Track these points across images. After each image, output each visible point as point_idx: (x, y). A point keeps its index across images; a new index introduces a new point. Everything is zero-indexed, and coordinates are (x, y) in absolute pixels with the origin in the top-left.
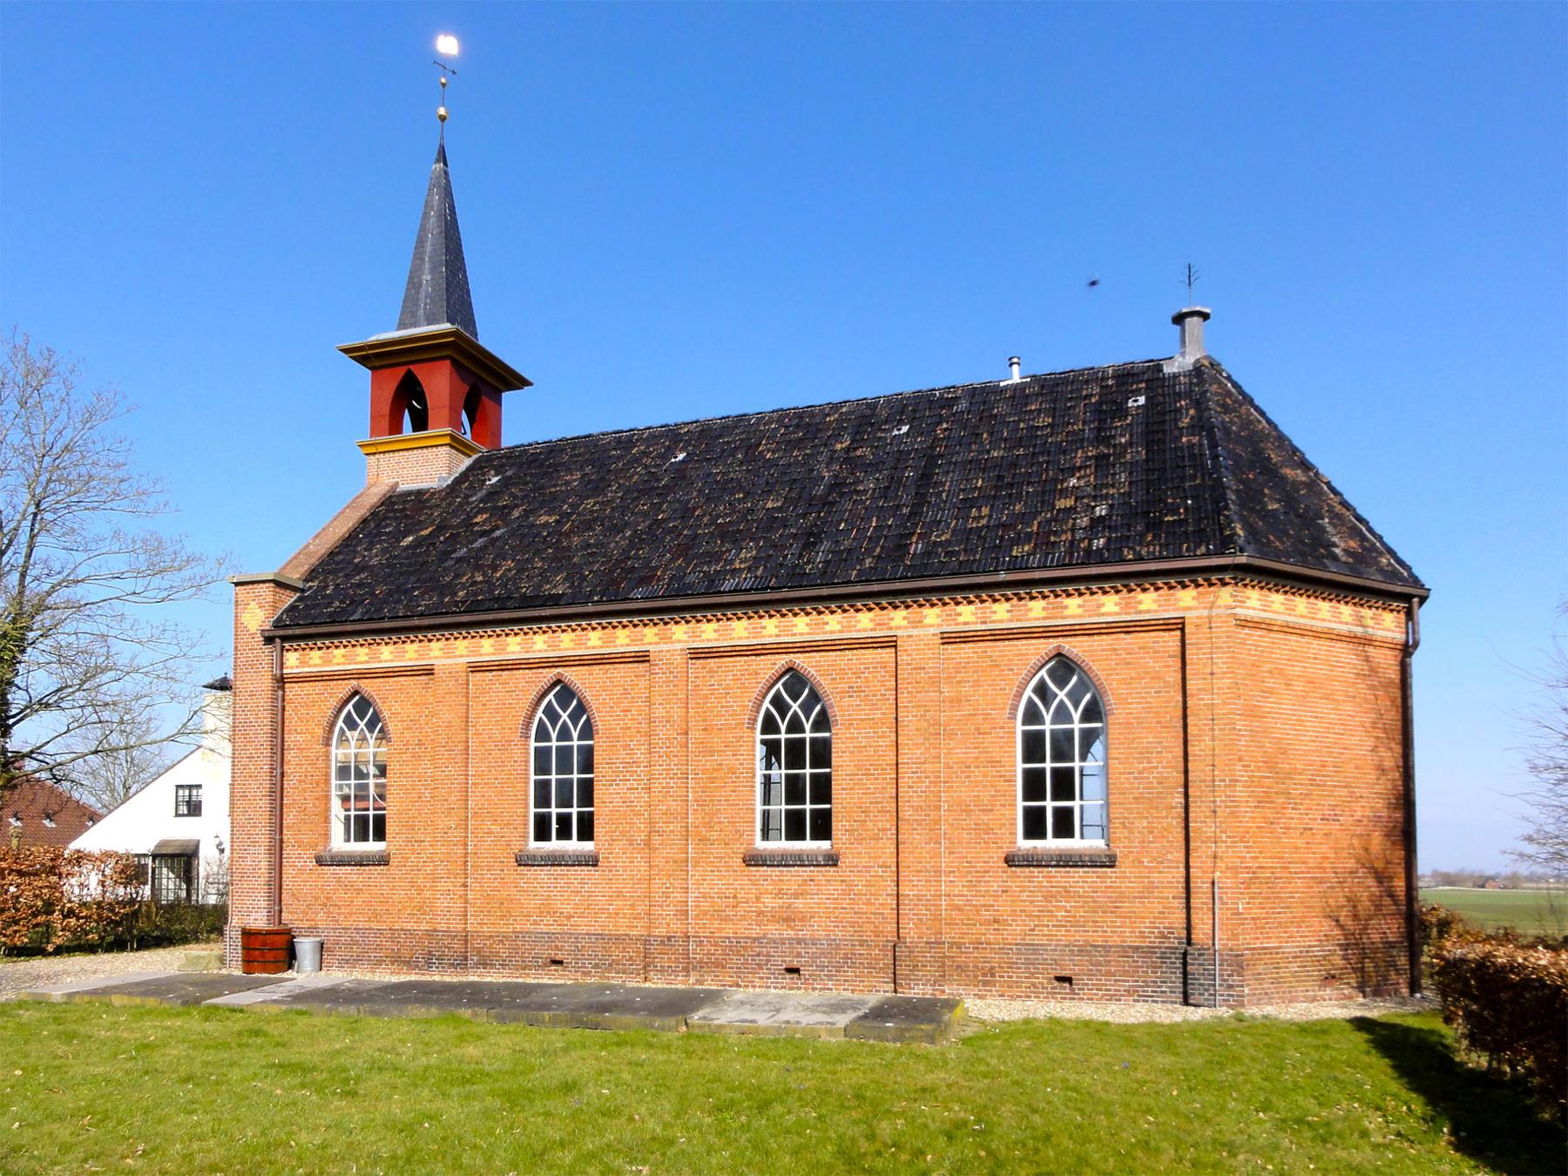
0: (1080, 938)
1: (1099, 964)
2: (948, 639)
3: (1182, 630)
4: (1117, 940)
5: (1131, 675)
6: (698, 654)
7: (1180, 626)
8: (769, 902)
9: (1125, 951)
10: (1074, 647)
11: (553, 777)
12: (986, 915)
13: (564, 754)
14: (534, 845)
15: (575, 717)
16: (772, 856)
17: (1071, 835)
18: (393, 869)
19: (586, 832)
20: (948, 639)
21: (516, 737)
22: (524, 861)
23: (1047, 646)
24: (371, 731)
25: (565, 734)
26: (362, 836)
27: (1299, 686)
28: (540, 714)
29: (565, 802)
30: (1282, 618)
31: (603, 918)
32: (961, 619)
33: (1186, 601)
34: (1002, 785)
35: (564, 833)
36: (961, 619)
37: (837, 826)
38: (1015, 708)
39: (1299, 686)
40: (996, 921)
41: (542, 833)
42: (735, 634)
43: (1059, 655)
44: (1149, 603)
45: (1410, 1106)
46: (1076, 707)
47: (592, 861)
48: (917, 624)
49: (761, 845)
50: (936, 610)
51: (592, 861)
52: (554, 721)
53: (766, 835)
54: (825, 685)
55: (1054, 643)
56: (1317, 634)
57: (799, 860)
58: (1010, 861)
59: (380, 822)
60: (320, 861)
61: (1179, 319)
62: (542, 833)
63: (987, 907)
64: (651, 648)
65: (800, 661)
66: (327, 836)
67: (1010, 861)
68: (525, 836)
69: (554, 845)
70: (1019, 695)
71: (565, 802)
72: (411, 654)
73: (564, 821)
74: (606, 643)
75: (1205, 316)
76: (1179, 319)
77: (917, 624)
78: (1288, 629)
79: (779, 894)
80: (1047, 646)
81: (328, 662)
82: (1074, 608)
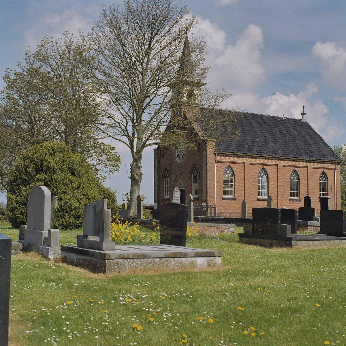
7: (307, 168)
20: (314, 168)
29: (323, 191)
33: (245, 160)
65: (296, 169)
72: (241, 160)
77: (310, 165)
80: (322, 171)
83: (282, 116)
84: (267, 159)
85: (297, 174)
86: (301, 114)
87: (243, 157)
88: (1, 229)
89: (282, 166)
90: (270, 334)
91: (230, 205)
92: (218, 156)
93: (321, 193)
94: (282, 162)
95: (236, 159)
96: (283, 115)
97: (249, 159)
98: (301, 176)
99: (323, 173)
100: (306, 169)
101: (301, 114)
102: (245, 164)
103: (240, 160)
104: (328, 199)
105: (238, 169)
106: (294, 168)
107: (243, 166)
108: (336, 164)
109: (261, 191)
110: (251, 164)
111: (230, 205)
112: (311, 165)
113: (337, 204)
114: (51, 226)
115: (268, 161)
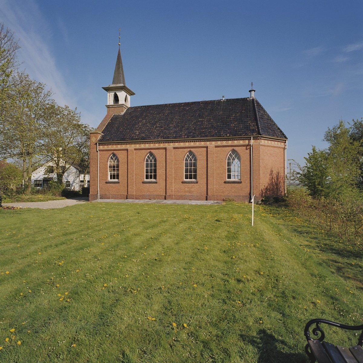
0: (236, 194)
1: (239, 198)
2: (216, 147)
3: (127, 151)
4: (242, 195)
5: (200, 154)
6: (174, 148)
9: (243, 197)
10: (236, 148)
11: (189, 168)
12: (222, 191)
13: (191, 164)
14: (146, 180)
15: (192, 157)
16: (187, 182)
17: (230, 178)
18: (120, 184)
19: (155, 178)
20: (216, 147)
21: (143, 161)
22: (143, 183)
24: (116, 160)
25: (191, 160)
26: (114, 178)
28: (147, 157)
29: (151, 172)
30: (267, 144)
31: (158, 192)
32: (218, 144)
33: (128, 147)
35: (151, 178)
36: (218, 144)
37: (198, 177)
38: (144, 159)
39: (269, 155)
40: (223, 192)
42: (181, 145)
43: (233, 149)
44: (162, 145)
46: (236, 158)
47: (156, 183)
49: (146, 180)
50: (143, 145)
51: (156, 183)
53: (111, 179)
54: (196, 154)
55: (233, 148)
56: (272, 147)
57: (192, 182)
58: (225, 182)
59: (118, 175)
60: (106, 183)
61: (250, 91)
62: (147, 178)
63: (222, 190)
64: (167, 147)
66: (107, 178)
67: (225, 182)
68: (144, 178)
70: (227, 156)
71: (151, 172)
72: (161, 145)
73: (151, 176)
74: (116, 147)
75: (255, 91)
76: (250, 91)
78: (268, 146)
80: (111, 152)
81: (116, 147)
82: (236, 143)
83: (222, 98)
84: (242, 140)
85: (194, 156)
87: (126, 143)
88: (357, 255)
91: (114, 188)
92: (253, 139)
94: (172, 144)
95: (119, 147)
97: (133, 145)
98: (199, 157)
103: (124, 147)
104: (152, 179)
105: (121, 156)
106: (189, 149)
107: (248, 151)
108: (251, 139)
110: (135, 149)
111: (114, 188)
112: (211, 145)
113: (255, 186)
115: (268, 143)
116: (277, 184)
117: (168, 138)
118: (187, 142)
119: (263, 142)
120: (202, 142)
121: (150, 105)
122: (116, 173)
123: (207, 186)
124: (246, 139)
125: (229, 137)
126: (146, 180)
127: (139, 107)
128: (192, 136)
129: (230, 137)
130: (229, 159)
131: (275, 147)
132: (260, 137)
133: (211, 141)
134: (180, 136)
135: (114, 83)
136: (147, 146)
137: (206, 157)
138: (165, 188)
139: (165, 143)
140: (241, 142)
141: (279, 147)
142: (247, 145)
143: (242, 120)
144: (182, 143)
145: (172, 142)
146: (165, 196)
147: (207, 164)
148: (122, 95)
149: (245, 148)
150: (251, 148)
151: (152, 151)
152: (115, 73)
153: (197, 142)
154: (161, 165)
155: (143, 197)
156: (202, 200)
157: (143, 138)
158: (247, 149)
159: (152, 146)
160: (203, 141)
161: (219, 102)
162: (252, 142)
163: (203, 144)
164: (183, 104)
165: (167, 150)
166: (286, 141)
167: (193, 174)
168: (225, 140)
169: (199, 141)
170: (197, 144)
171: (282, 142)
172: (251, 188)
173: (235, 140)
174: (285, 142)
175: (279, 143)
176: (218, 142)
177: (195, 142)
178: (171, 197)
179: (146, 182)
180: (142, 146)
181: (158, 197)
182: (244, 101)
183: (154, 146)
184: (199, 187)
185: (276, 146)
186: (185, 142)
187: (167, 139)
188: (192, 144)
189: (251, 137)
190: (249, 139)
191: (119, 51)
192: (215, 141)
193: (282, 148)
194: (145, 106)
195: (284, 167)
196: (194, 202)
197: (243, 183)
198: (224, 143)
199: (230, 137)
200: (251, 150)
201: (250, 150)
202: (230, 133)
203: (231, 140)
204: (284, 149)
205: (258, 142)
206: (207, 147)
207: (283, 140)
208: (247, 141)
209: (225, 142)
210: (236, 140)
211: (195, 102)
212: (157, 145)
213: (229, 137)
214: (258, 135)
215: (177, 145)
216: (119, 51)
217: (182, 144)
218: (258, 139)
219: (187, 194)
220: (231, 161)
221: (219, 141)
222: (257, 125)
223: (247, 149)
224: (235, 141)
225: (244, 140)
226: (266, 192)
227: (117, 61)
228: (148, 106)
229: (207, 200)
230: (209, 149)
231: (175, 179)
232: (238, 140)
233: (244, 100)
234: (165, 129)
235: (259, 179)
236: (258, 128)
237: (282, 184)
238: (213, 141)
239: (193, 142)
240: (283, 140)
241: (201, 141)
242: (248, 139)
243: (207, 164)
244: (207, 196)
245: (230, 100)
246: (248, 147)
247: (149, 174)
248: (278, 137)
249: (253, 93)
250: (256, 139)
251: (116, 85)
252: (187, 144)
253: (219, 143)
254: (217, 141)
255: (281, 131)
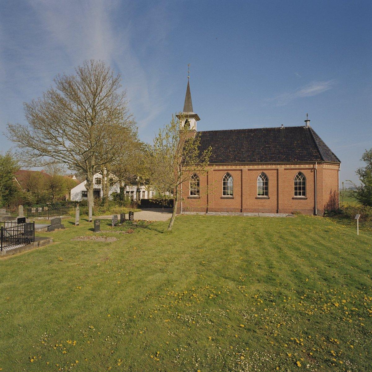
2: (285, 169)
5: (309, 175)
6: (249, 170)
7: (241, 170)
8: (259, 204)
12: (290, 205)
14: (223, 196)
20: (214, 170)
22: (221, 198)
23: (298, 171)
27: (328, 176)
33: (242, 167)
34: (292, 189)
37: (269, 194)
38: (222, 178)
41: (296, 194)
42: (255, 167)
44: (238, 167)
45: (70, 224)
48: (281, 167)
49: (223, 196)
52: (226, 178)
54: (267, 175)
56: (330, 169)
57: (264, 198)
58: (256, 198)
59: (198, 192)
60: (188, 198)
63: (290, 204)
65: (264, 171)
69: (298, 196)
75: (309, 121)
77: (281, 167)
79: (261, 203)
80: (298, 171)
83: (281, 126)
84: (308, 164)
86: (305, 121)
89: (247, 171)
90: (360, 316)
93: (265, 191)
94: (247, 167)
96: (282, 125)
98: (269, 178)
99: (300, 174)
100: (240, 171)
101: (305, 121)
102: (243, 170)
107: (313, 173)
108: (315, 164)
109: (226, 191)
112: (281, 168)
113: (318, 202)
114: (133, 215)
115: (332, 166)
116: (334, 201)
117: (244, 161)
118: (260, 165)
119: (325, 166)
120: (273, 166)
121: (217, 130)
122: (196, 190)
123: (278, 201)
124: (311, 164)
125: (297, 162)
126: (224, 196)
127: (207, 132)
128: (264, 160)
129: (298, 162)
130: (224, 180)
131: (332, 169)
132: (323, 162)
133: (281, 165)
134: (254, 160)
135: (184, 110)
136: (225, 168)
137: (276, 178)
138: (240, 203)
139: (241, 165)
140: (307, 166)
141: (335, 170)
142: (312, 169)
143: (299, 146)
144: (251, 166)
145: (248, 165)
146: (241, 210)
147: (278, 183)
148: (192, 121)
149: (310, 170)
150: (315, 171)
151: (229, 172)
152: (185, 102)
153: (269, 165)
154: (238, 183)
155: (221, 210)
156: (274, 213)
157: (221, 161)
158: (311, 172)
159: (229, 167)
160: (274, 165)
161: (279, 130)
162: (316, 166)
163: (274, 167)
164: (247, 131)
165: (243, 172)
166: (339, 164)
167: (302, 186)
168: (293, 164)
169: (271, 165)
170: (269, 167)
171: (337, 165)
172: (315, 203)
173: (301, 164)
174: (340, 165)
175: (335, 166)
176: (287, 165)
177: (267, 165)
178: (247, 211)
179: (223, 198)
180: (221, 168)
181: (234, 210)
182: (301, 129)
183: (231, 168)
184: (271, 202)
185: (333, 168)
186: (259, 165)
187: (242, 161)
188: (265, 167)
189: (316, 162)
190: (314, 164)
191: (188, 83)
192: (285, 165)
193: (336, 170)
194: (213, 131)
195: (338, 185)
196: (267, 215)
197: (308, 199)
198: (293, 167)
199: (298, 162)
200: (315, 173)
201: (315, 173)
202: (297, 158)
203: (298, 164)
204: (338, 170)
205: (321, 166)
206: (277, 170)
207: (338, 164)
208: (312, 166)
209: (293, 165)
210: (303, 164)
211: (257, 129)
212: (234, 167)
213: (297, 162)
214: (321, 160)
215: (251, 167)
216: (188, 83)
217: (256, 167)
218: (321, 164)
219: (260, 208)
220: (226, 181)
221: (288, 165)
222: (319, 151)
223: (311, 172)
224: (302, 165)
225: (309, 164)
226: (327, 208)
227: (187, 92)
228: (215, 131)
229: (277, 212)
230: (279, 171)
231: (250, 195)
232: (305, 164)
233: (301, 128)
234: (238, 153)
235: (322, 196)
236: (320, 154)
237: (336, 201)
238: (283, 165)
239: (265, 165)
240: (338, 164)
241: (272, 165)
242: (313, 164)
243: (278, 183)
244: (278, 210)
245: (289, 128)
246: (313, 170)
247: (298, 186)
248: (335, 162)
249: (308, 122)
250: (320, 164)
251: (188, 113)
252: (260, 167)
253: (288, 166)
254: (286, 165)
255: (335, 156)
